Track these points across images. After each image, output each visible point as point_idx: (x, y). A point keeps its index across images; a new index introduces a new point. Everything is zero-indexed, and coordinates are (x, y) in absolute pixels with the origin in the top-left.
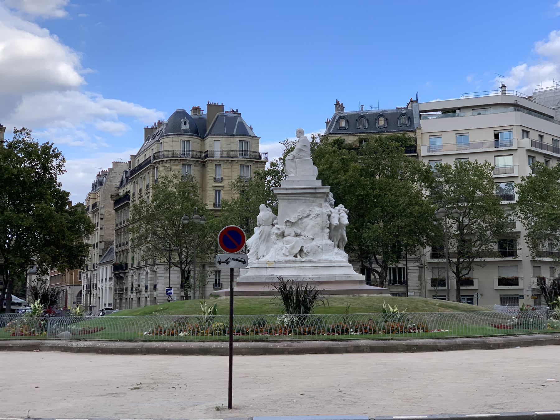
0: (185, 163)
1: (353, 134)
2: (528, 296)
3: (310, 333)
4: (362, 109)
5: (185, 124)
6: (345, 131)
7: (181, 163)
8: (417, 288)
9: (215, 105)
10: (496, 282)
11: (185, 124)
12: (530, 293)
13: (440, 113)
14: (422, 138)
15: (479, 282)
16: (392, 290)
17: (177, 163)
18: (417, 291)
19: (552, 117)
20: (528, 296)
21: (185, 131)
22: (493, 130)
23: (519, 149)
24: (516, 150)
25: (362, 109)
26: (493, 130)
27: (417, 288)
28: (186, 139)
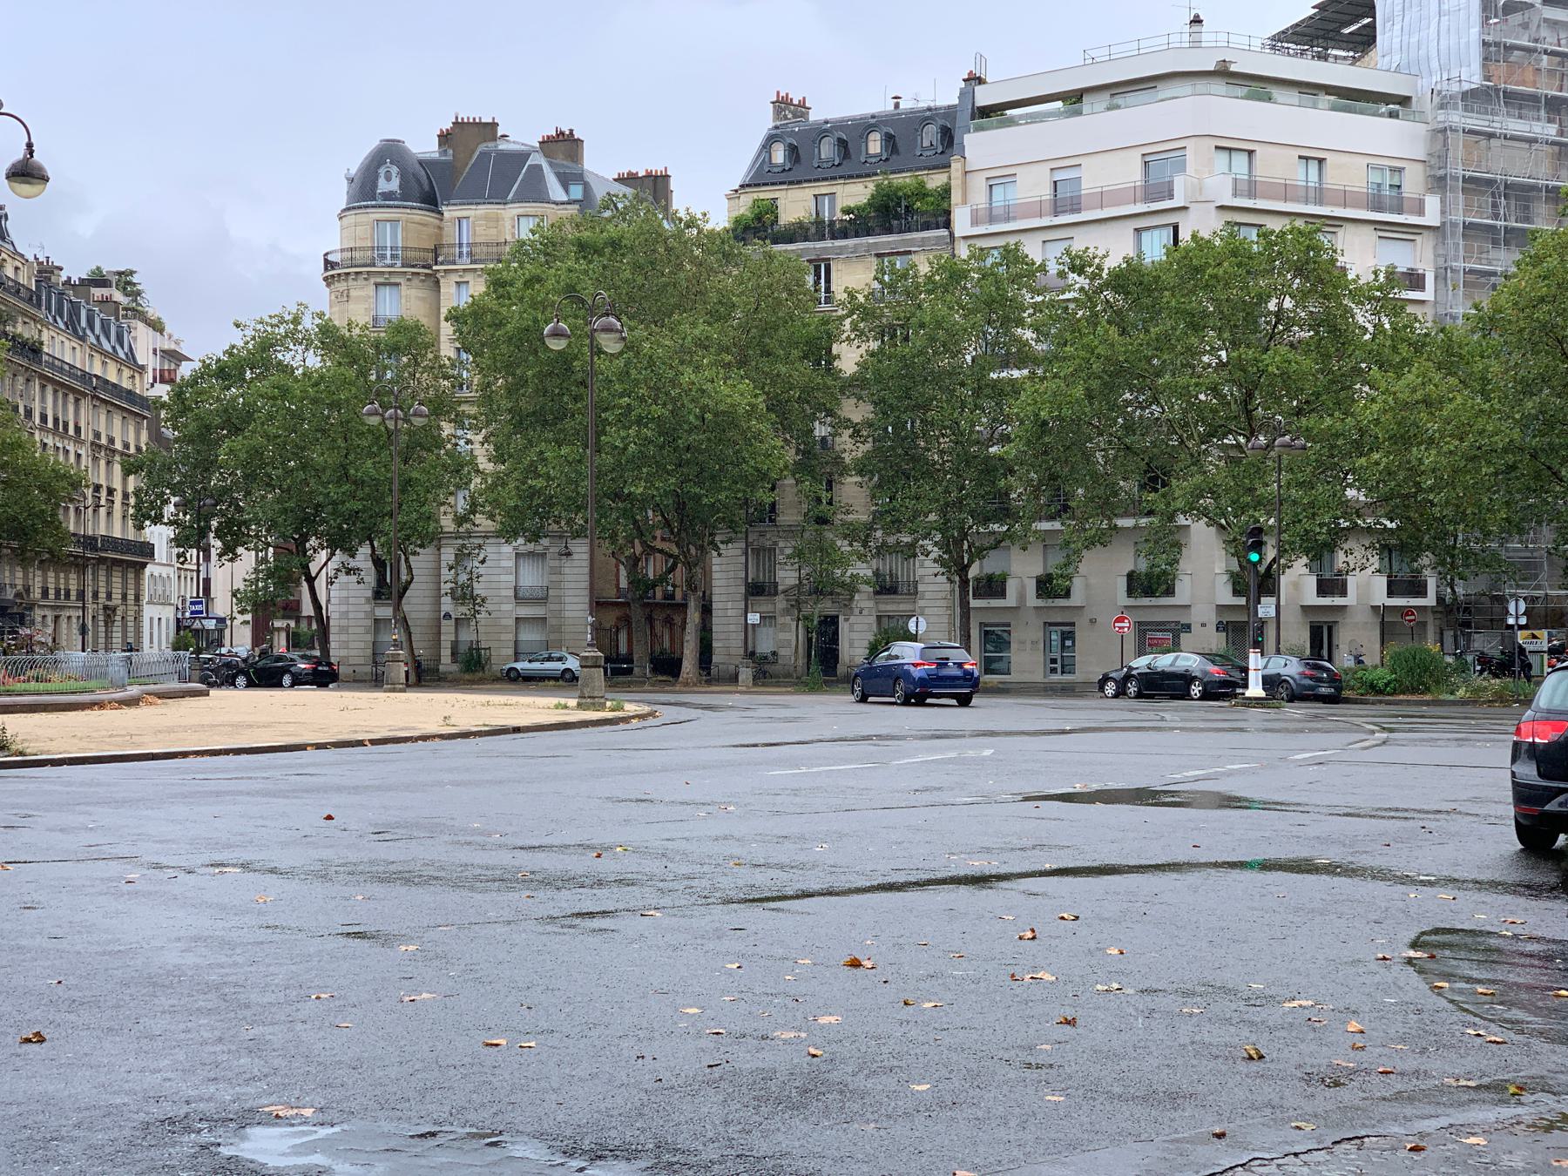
0: (381, 280)
1: (799, 182)
2: (1203, 625)
3: (481, 681)
4: (897, 106)
5: (388, 179)
6: (783, 177)
7: (372, 280)
8: (944, 603)
9: (475, 123)
10: (1122, 583)
11: (388, 179)
12: (1212, 618)
13: (1059, 104)
14: (964, 183)
15: (1087, 586)
16: (882, 607)
17: (361, 282)
18: (942, 611)
19: (1404, 101)
20: (1203, 625)
21: (388, 196)
22: (1138, 152)
23: (1192, 206)
24: (1185, 208)
25: (897, 106)
26: (1138, 152)
27: (944, 603)
28: (824, 191)
